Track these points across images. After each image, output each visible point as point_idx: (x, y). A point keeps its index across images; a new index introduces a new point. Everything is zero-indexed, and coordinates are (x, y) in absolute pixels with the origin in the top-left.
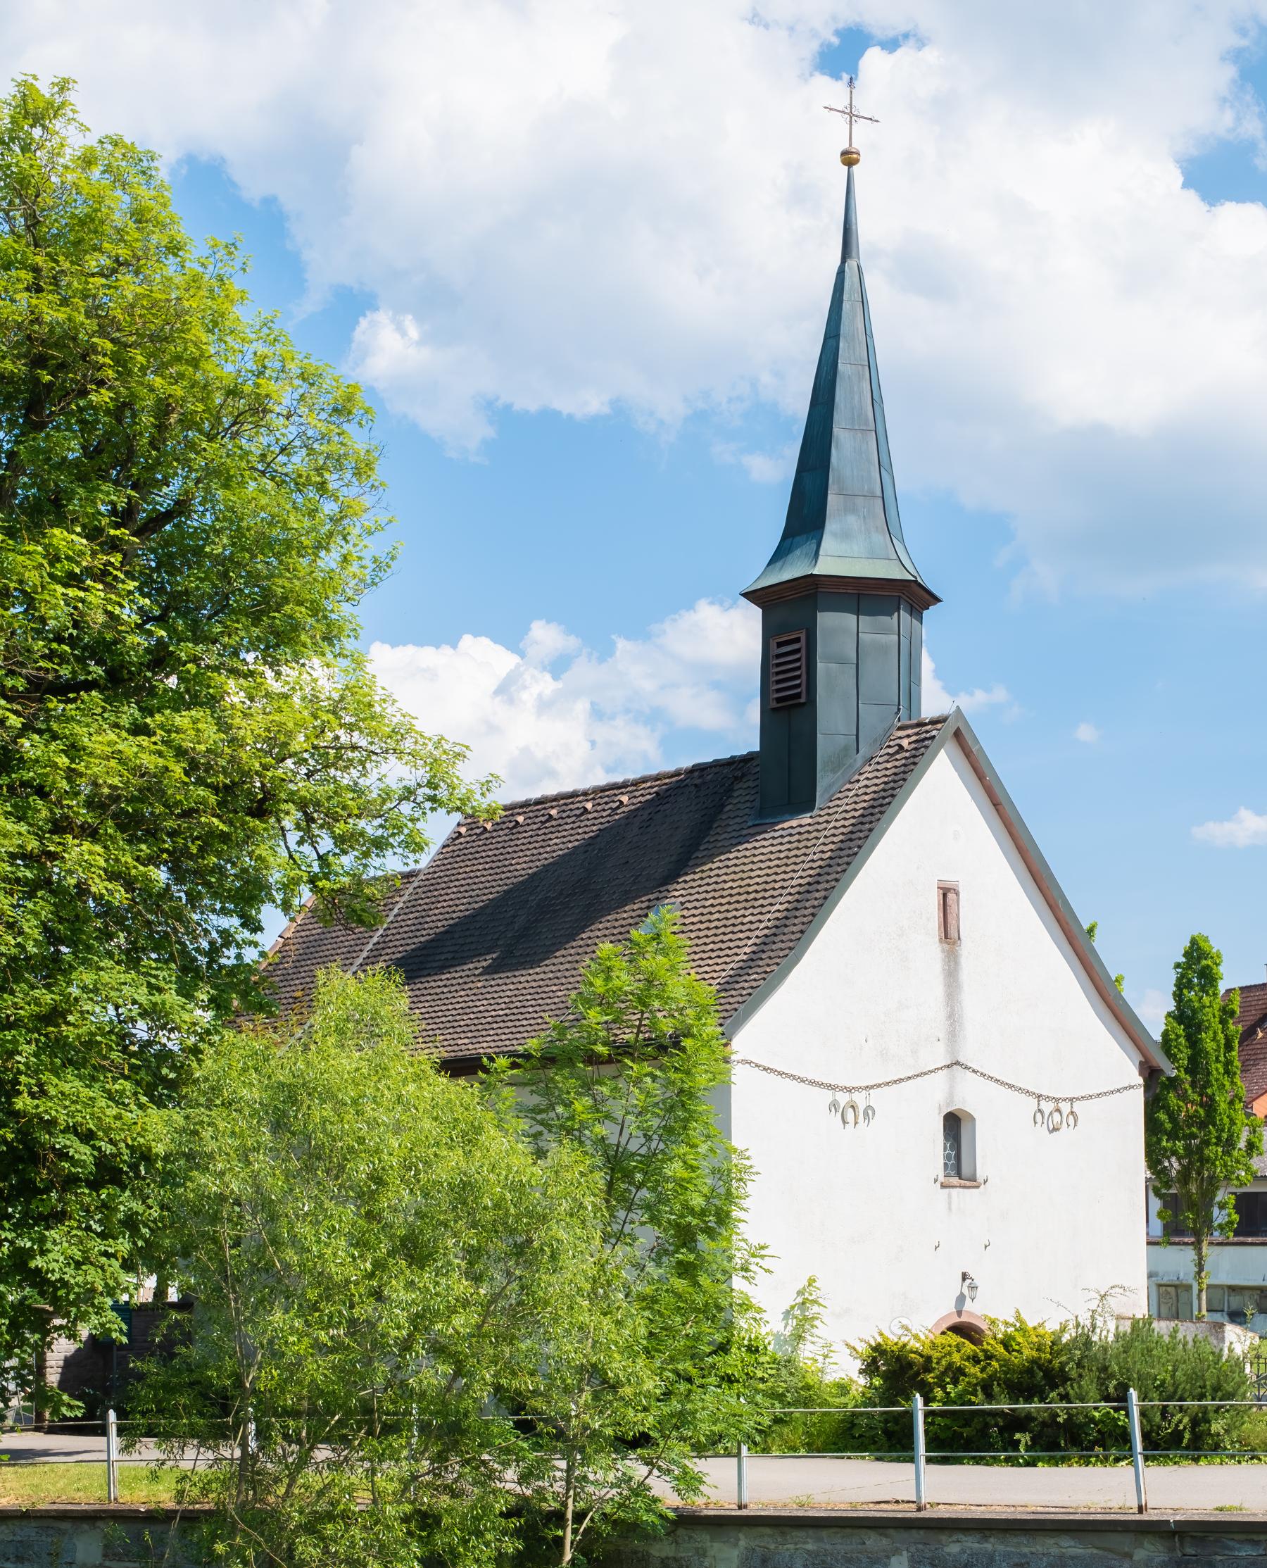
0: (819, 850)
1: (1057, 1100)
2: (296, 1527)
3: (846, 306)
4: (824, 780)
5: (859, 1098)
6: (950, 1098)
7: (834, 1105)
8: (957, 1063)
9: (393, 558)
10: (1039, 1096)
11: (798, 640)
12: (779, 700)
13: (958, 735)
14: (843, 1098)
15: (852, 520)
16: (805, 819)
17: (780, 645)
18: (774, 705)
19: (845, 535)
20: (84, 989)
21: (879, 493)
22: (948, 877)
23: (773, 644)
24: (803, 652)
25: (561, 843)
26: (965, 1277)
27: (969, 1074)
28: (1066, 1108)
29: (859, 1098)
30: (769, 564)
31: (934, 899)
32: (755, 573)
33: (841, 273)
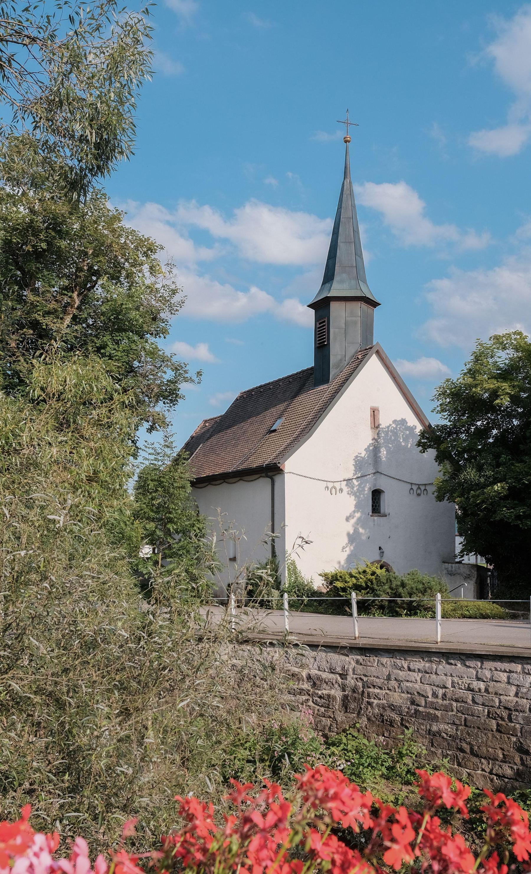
1: (419, 485)
2: (444, 497)
4: (332, 372)
6: (375, 485)
8: (378, 472)
11: (324, 322)
12: (319, 344)
13: (378, 352)
15: (344, 275)
16: (326, 386)
17: (320, 324)
18: (318, 345)
19: (341, 282)
20: (177, 822)
21: (355, 265)
22: (375, 405)
23: (318, 324)
25: (214, 483)
26: (380, 548)
27: (382, 476)
28: (423, 488)
30: (323, 284)
31: (368, 413)
32: (313, 296)
33: (343, 183)
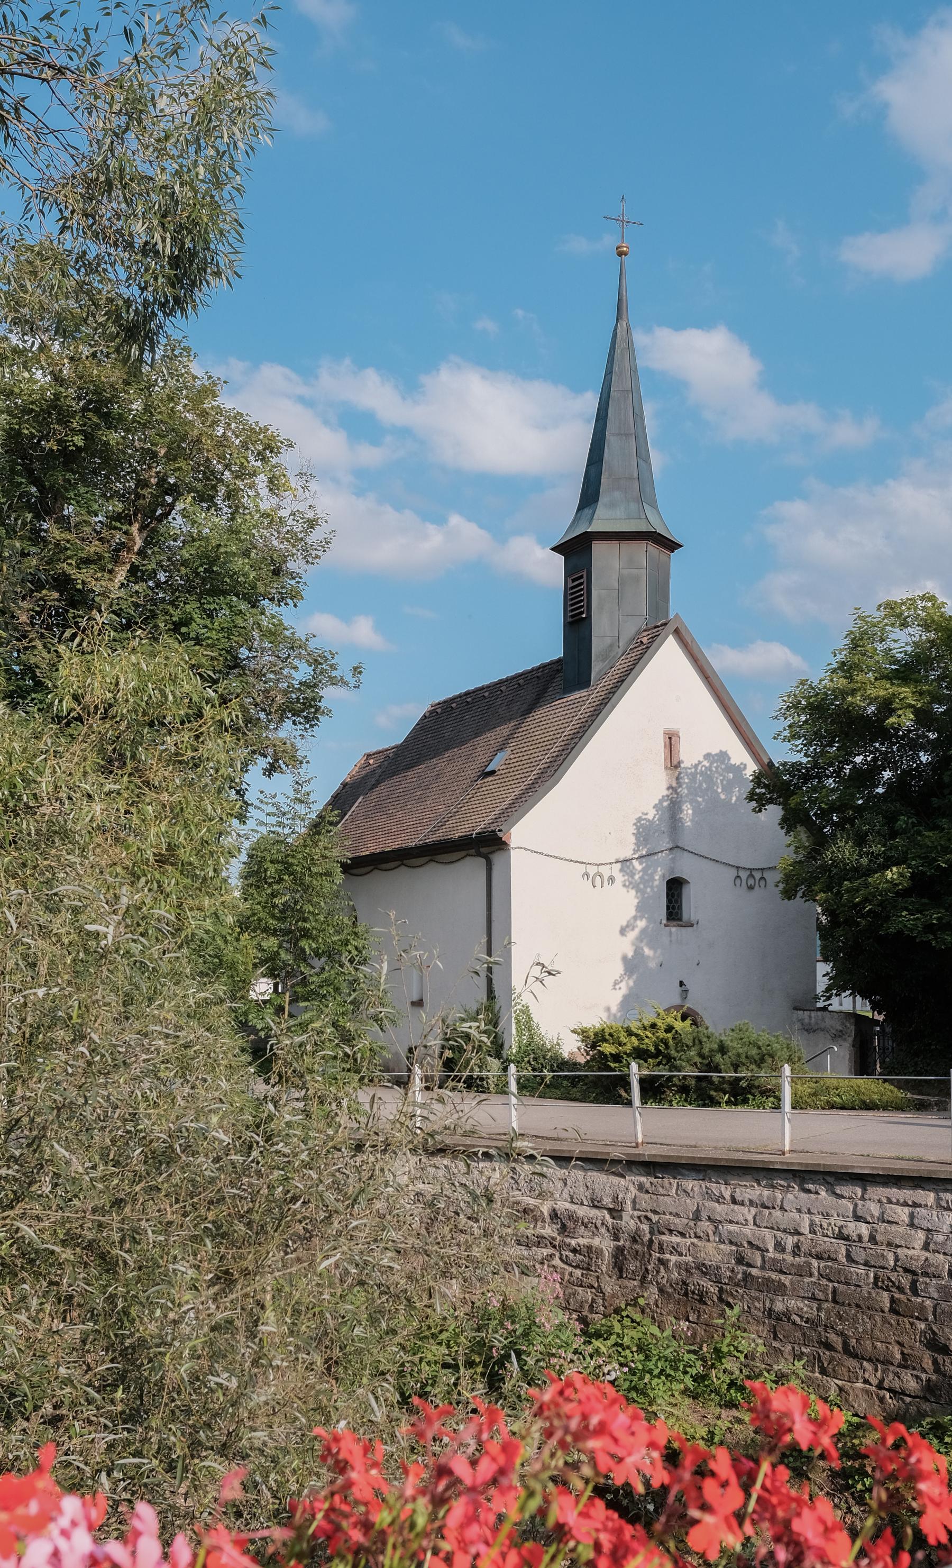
0: (585, 710)
3: (618, 351)
5: (603, 869)
6: (672, 870)
7: (586, 874)
8: (677, 847)
9: (328, 543)
10: (738, 868)
11: (581, 577)
12: (572, 616)
14: (592, 870)
15: (617, 495)
16: (583, 693)
17: (573, 581)
18: (569, 620)
19: (612, 505)
21: (636, 475)
22: (672, 726)
23: (570, 580)
24: (584, 580)
26: (681, 984)
29: (603, 869)
31: (661, 741)
32: (561, 532)
33: (616, 329)
